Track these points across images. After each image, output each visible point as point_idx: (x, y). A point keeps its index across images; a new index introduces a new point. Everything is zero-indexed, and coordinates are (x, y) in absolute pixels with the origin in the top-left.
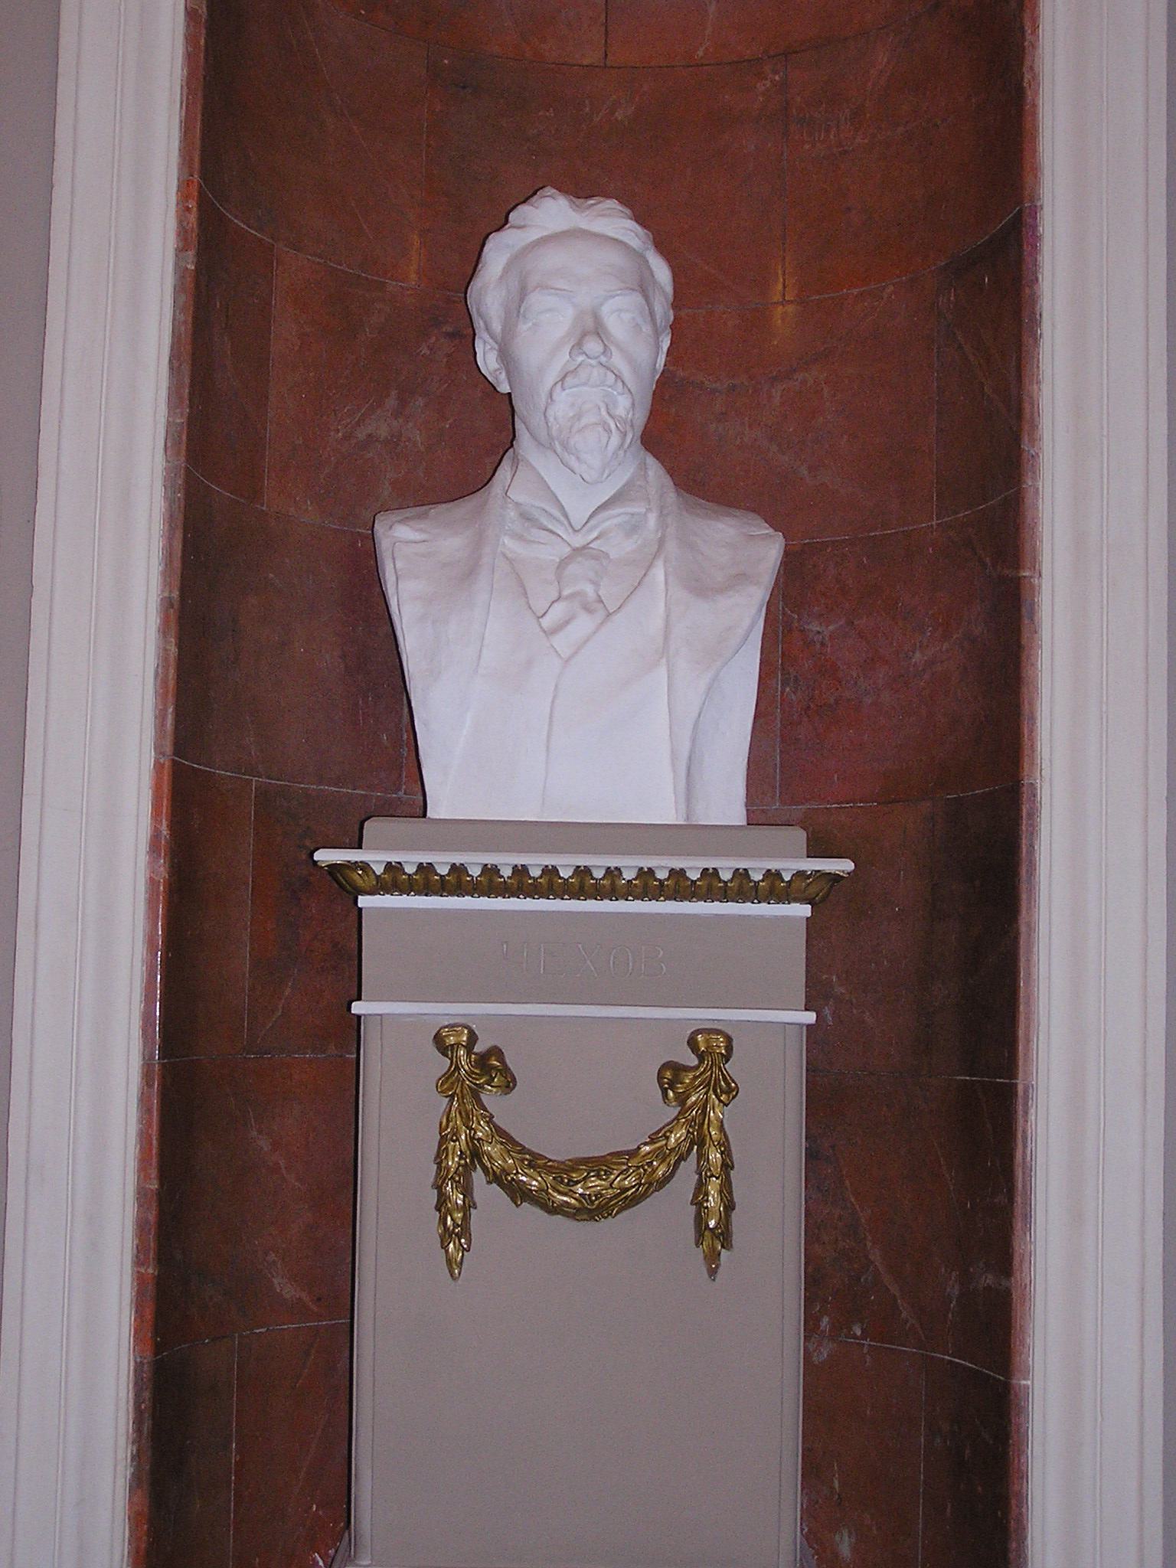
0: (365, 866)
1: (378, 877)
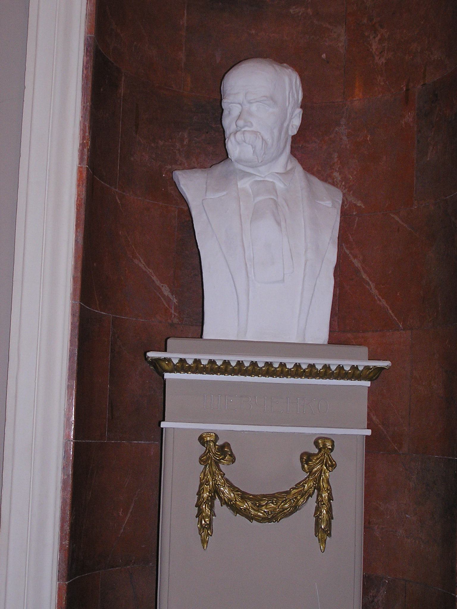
0: (169, 360)
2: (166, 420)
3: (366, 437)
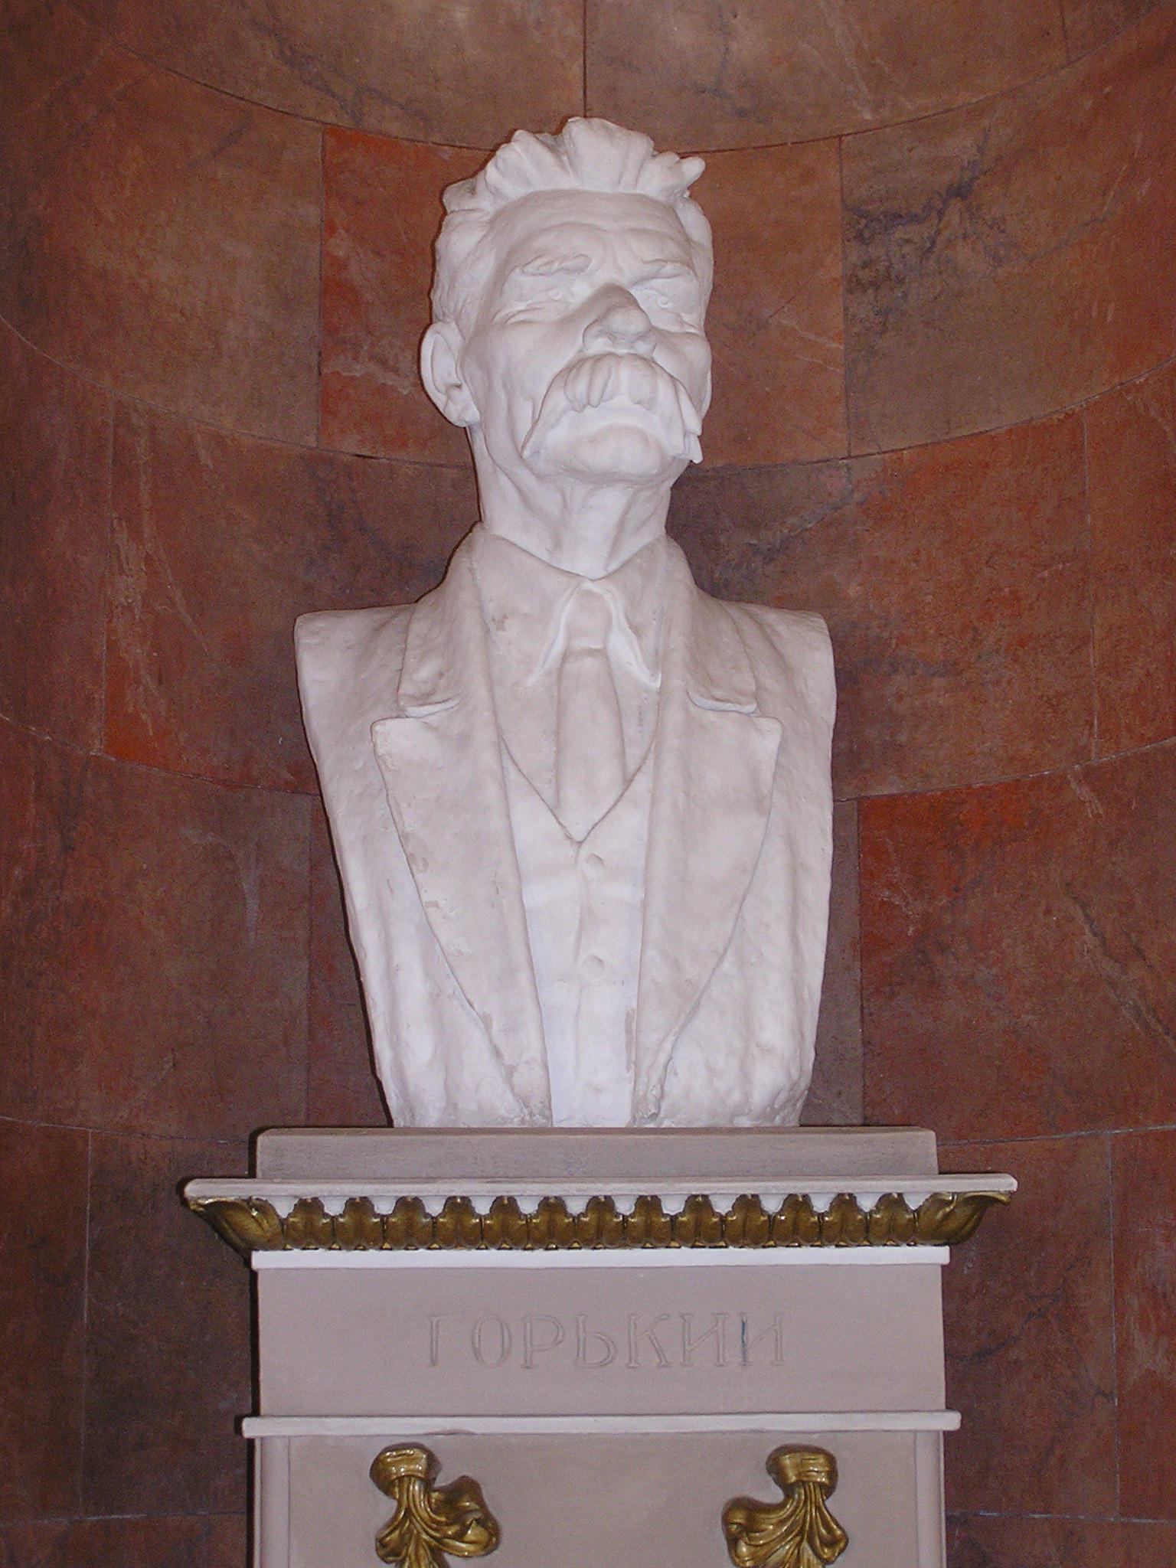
0: (264, 1208)
1: (283, 1222)
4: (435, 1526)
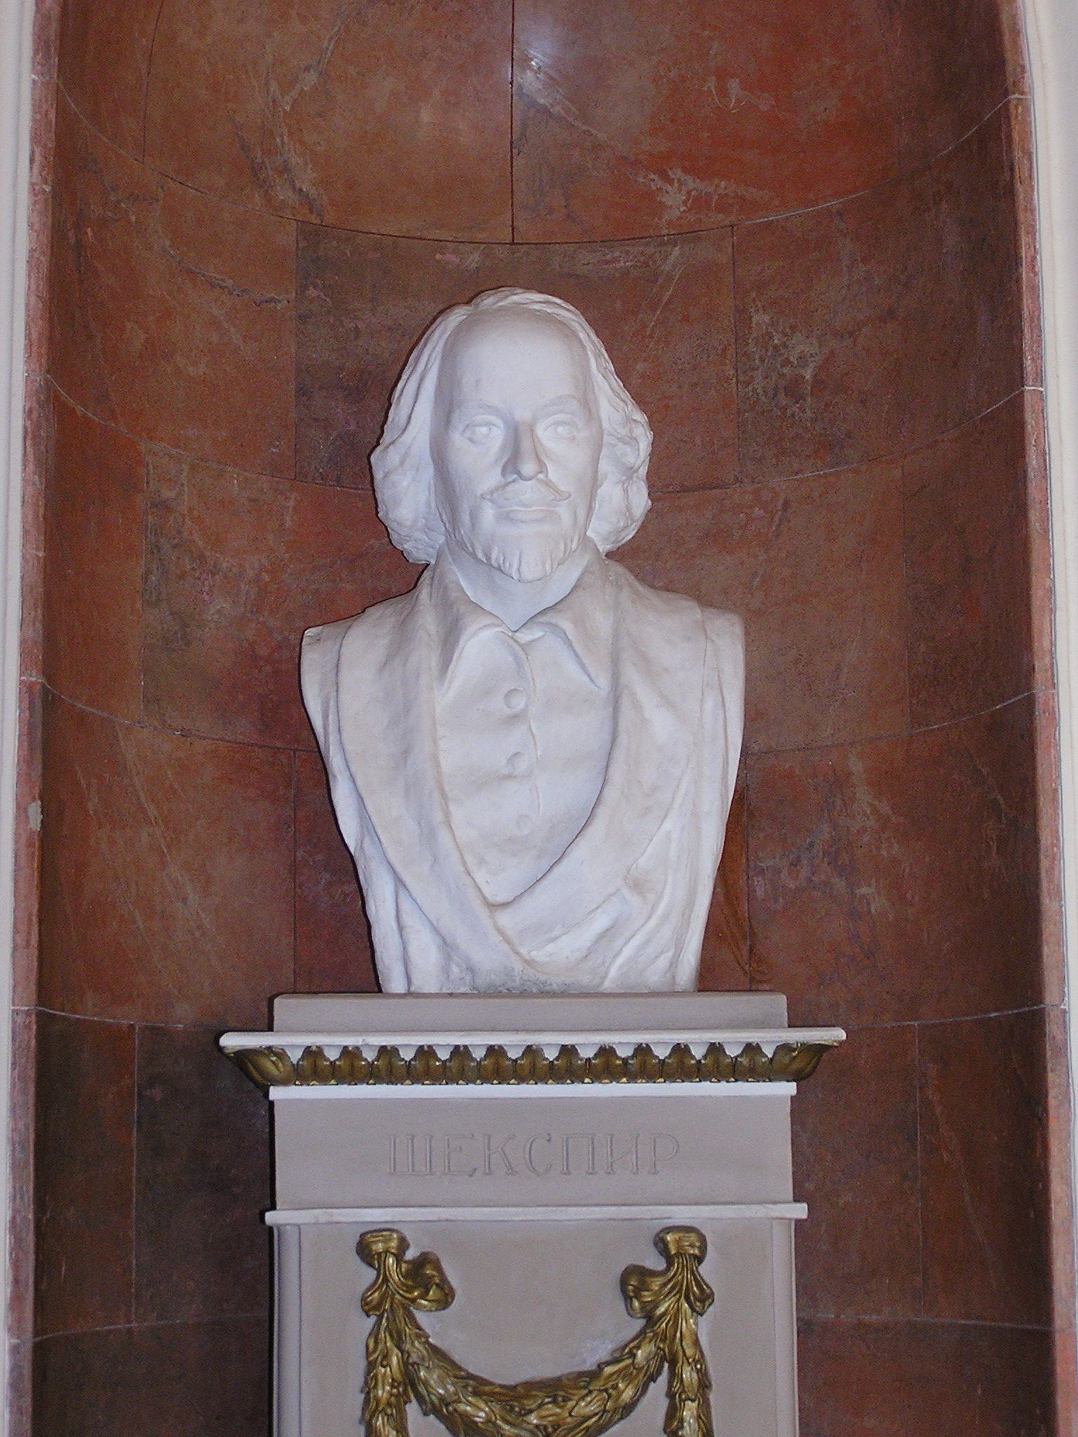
0: (280, 1054)
2: (278, 1208)
3: (796, 1225)
4: (405, 1289)
